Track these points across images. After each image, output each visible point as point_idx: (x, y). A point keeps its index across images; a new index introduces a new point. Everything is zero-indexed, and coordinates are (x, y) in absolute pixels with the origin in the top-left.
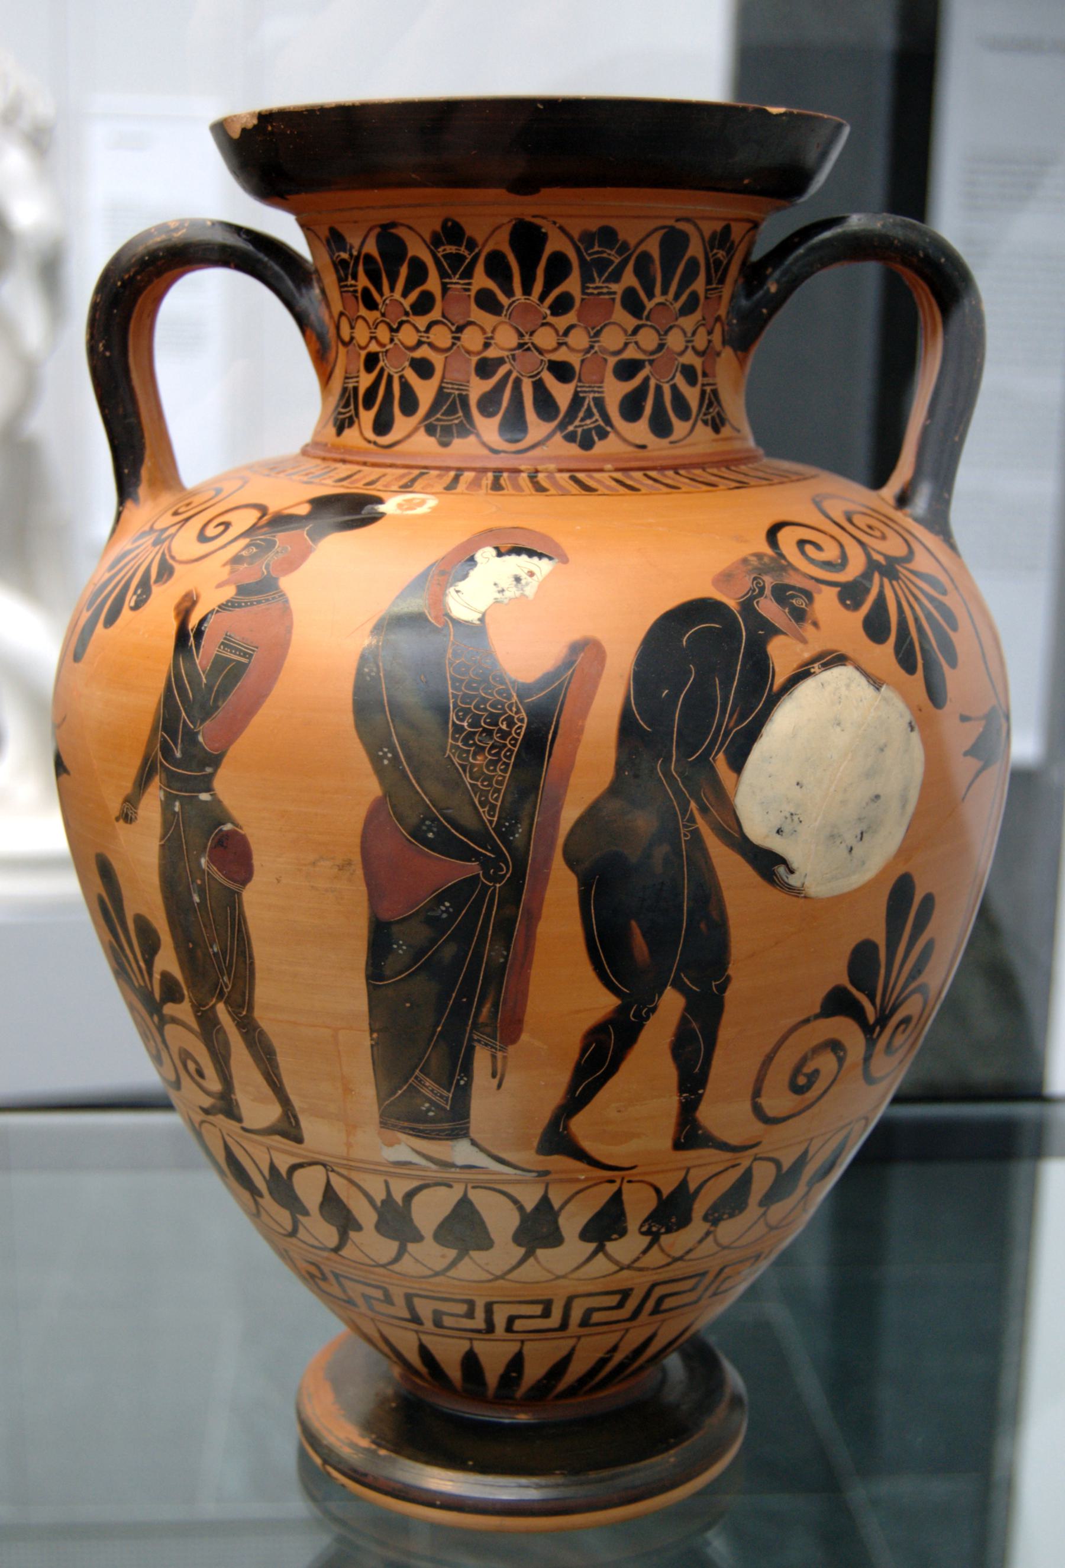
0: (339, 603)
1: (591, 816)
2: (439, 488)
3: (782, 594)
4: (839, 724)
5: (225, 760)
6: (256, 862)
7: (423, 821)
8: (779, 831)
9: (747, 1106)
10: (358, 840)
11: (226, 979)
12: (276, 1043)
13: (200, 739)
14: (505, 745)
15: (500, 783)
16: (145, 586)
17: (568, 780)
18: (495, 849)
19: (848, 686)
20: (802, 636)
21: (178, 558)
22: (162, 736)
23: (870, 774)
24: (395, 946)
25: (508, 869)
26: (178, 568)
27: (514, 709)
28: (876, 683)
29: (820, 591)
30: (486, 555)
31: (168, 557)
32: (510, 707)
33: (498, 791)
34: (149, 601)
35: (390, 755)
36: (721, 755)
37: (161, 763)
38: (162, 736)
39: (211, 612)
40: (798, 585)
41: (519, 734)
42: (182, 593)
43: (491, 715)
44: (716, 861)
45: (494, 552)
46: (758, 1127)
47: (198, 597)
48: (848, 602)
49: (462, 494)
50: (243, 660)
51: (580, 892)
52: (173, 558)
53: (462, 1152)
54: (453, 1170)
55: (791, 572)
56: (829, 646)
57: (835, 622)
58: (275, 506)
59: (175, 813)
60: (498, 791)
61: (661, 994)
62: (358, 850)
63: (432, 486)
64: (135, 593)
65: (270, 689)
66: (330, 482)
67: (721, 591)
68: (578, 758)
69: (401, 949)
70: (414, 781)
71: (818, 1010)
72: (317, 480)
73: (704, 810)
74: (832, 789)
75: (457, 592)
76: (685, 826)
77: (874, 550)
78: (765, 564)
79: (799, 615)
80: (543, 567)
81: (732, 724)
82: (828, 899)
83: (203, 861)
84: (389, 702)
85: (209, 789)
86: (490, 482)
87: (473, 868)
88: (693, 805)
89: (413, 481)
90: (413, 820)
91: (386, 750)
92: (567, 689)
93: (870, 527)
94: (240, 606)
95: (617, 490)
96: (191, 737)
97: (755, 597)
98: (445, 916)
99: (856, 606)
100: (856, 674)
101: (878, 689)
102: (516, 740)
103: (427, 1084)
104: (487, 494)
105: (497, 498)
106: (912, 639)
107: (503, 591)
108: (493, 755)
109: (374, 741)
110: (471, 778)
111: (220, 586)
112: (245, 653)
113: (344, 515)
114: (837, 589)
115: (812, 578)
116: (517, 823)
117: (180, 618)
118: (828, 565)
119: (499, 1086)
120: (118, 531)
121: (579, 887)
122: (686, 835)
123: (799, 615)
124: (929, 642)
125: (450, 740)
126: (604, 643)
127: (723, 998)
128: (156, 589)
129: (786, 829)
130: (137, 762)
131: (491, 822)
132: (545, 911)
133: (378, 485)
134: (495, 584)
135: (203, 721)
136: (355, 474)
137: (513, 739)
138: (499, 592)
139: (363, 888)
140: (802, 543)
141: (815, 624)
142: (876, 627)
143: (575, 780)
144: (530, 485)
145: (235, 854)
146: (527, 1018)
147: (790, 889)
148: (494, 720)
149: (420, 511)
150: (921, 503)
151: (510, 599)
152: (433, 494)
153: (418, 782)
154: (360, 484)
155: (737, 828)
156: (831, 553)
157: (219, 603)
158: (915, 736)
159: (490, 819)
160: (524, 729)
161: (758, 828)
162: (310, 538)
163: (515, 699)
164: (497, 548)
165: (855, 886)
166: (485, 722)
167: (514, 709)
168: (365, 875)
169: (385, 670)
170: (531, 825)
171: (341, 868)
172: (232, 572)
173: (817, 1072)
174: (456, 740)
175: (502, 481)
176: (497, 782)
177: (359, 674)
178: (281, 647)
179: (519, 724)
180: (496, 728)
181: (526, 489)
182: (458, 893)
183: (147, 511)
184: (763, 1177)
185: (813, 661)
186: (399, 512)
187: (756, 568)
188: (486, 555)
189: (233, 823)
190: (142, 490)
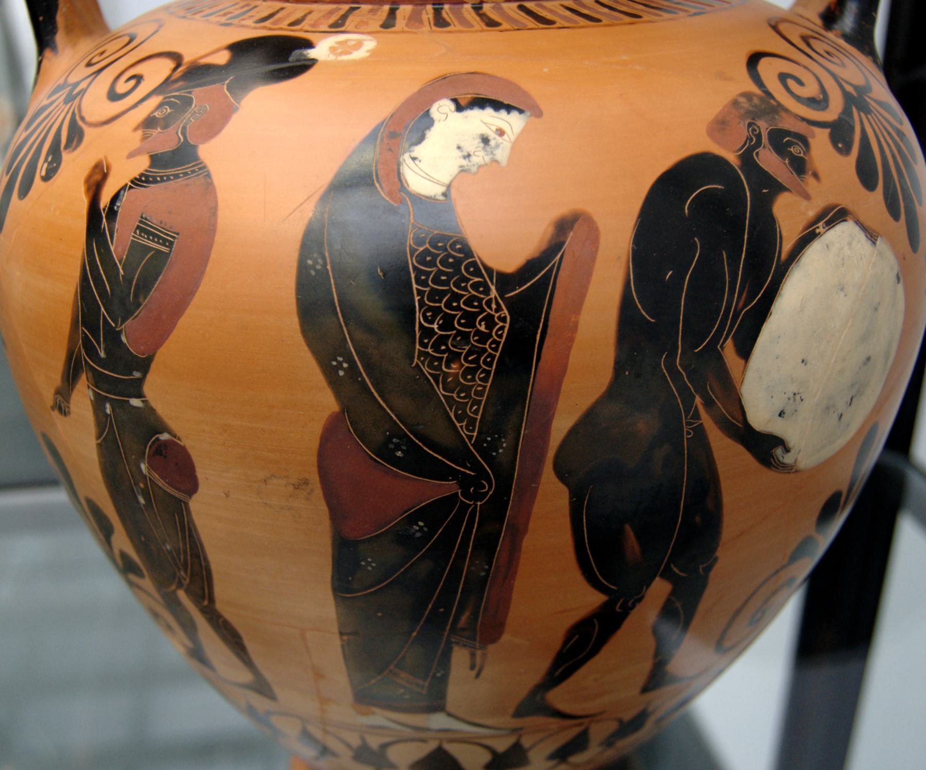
0: (273, 172)
2: (375, 25)
3: (781, 141)
4: (842, 289)
5: (154, 366)
6: (200, 473)
7: (389, 440)
10: (314, 459)
11: (182, 573)
12: (241, 630)
13: (124, 339)
14: (485, 350)
15: (480, 394)
16: (55, 152)
18: (477, 467)
21: (89, 118)
22: (83, 332)
23: (865, 337)
24: (363, 563)
25: (490, 487)
26: (87, 131)
27: (494, 306)
30: (442, 109)
31: (77, 118)
32: (489, 303)
33: (478, 403)
34: (60, 170)
35: (345, 365)
36: (729, 341)
37: (86, 362)
38: (83, 332)
39: (124, 188)
41: (500, 336)
42: (93, 163)
43: (466, 315)
44: (717, 454)
45: (452, 106)
47: (108, 168)
49: (403, 32)
50: (163, 249)
52: (82, 118)
53: (438, 721)
55: (783, 114)
58: (189, 55)
59: (107, 415)
63: (367, 24)
64: (46, 160)
65: (197, 286)
66: (249, 22)
67: (718, 143)
68: (571, 360)
69: (370, 565)
70: (376, 395)
72: (236, 21)
73: (709, 403)
75: (414, 159)
76: (688, 424)
78: (755, 106)
79: (799, 166)
80: (513, 123)
81: (741, 304)
83: (143, 467)
84: (339, 301)
85: (140, 395)
86: (431, 16)
87: (450, 487)
88: (698, 400)
89: (344, 17)
91: (340, 359)
92: (556, 278)
93: (828, 53)
94: (155, 182)
95: (576, 22)
96: (113, 337)
98: (418, 535)
100: (856, 229)
101: (874, 243)
102: (498, 343)
104: (432, 32)
105: (442, 37)
107: (469, 156)
108: (471, 362)
109: (326, 350)
110: (444, 389)
111: (131, 155)
112: (165, 240)
113: (269, 63)
114: (828, 130)
115: (803, 119)
116: (500, 437)
117: (91, 193)
118: (811, 102)
119: (478, 675)
120: (39, 80)
121: (571, 498)
122: (688, 433)
124: (906, 183)
125: (418, 347)
126: (596, 218)
128: (66, 156)
129: (787, 411)
130: (62, 355)
131: (470, 438)
132: (531, 525)
133: (305, 25)
134: (459, 148)
135: (124, 319)
136: (278, 12)
137: (494, 342)
138: (464, 157)
139: (324, 508)
143: (568, 385)
144: (478, 18)
145: (178, 466)
146: (509, 621)
148: (470, 319)
149: (359, 54)
150: (848, 21)
151: (480, 167)
152: (369, 33)
154: (284, 25)
155: (741, 418)
156: (810, 90)
157: (132, 177)
158: (900, 287)
161: (760, 414)
162: (230, 92)
163: (494, 293)
164: (455, 101)
166: (459, 323)
167: (494, 306)
169: (332, 262)
171: (296, 487)
172: (145, 138)
174: (425, 346)
175: (444, 15)
176: (476, 393)
177: (302, 270)
178: (207, 230)
179: (501, 324)
180: (473, 330)
181: (474, 23)
182: (433, 513)
183: (67, 60)
186: (332, 57)
187: (748, 112)
188: (442, 109)
189: (170, 432)
190: (60, 38)
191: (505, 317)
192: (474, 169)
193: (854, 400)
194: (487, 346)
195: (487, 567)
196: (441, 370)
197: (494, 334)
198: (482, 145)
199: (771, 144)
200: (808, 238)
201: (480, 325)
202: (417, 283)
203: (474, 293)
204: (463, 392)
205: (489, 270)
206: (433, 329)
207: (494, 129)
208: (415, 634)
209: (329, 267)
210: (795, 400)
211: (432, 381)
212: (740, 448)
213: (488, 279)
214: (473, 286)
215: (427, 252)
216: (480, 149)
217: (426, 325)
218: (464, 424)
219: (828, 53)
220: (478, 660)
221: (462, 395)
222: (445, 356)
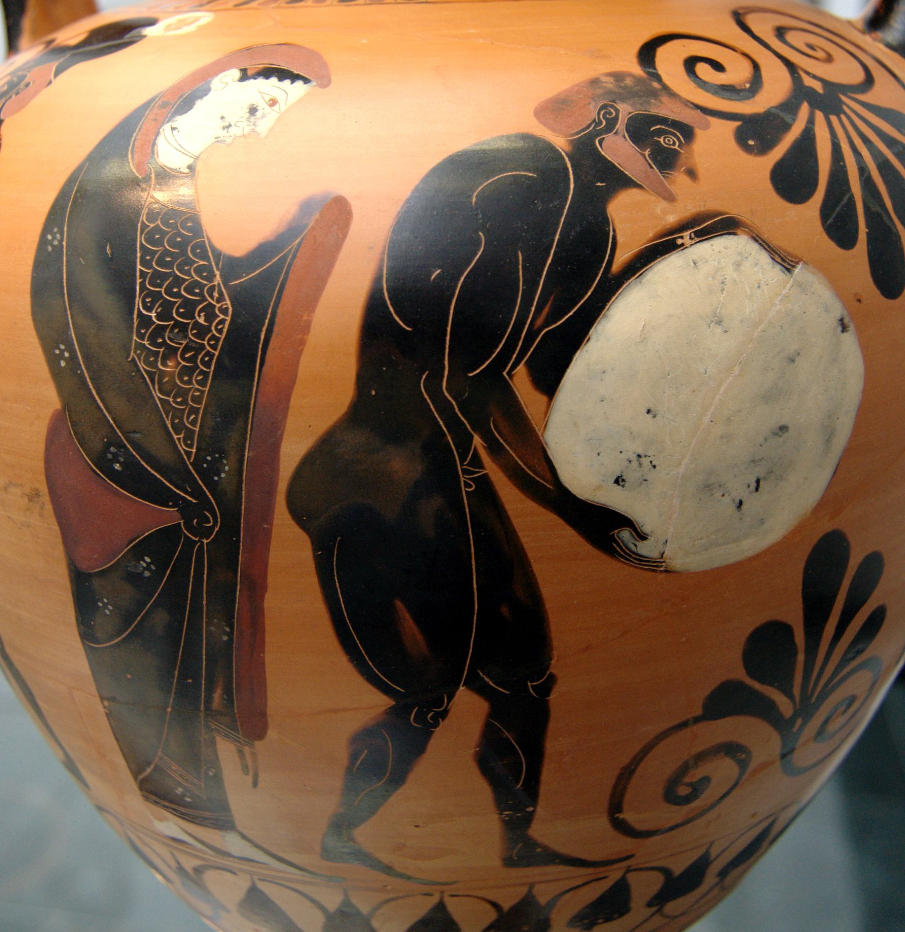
1: (324, 450)
3: (642, 130)
4: (719, 322)
8: (618, 481)
9: (603, 822)
17: (288, 399)
18: (196, 492)
19: (738, 265)
20: (667, 190)
23: (770, 396)
24: (100, 604)
27: (216, 295)
28: (786, 261)
29: (707, 126)
32: (211, 290)
36: (521, 369)
40: (672, 117)
43: (187, 303)
46: (625, 844)
48: (751, 142)
51: (316, 558)
54: (231, 859)
55: (665, 99)
56: (711, 205)
57: (723, 167)
60: (195, 411)
61: (451, 697)
62: (43, 478)
67: (545, 124)
68: (301, 368)
71: (699, 712)
73: (494, 448)
74: (706, 419)
76: (465, 472)
77: (808, 73)
78: (625, 87)
81: (539, 322)
82: (705, 573)
87: (170, 515)
88: (477, 441)
90: (97, 445)
92: (290, 266)
93: (812, 47)
97: (599, 133)
99: (764, 147)
100: (754, 247)
102: (218, 339)
103: (174, 768)
106: (852, 196)
110: (161, 391)
116: (221, 458)
118: (728, 90)
119: (255, 784)
121: (315, 550)
123: (665, 160)
125: (135, 338)
127: (547, 702)
129: (630, 477)
132: (271, 580)
137: (213, 337)
139: (56, 527)
140: (691, 63)
141: (692, 173)
142: (792, 180)
147: (642, 561)
148: (189, 308)
153: (98, 394)
155: (548, 475)
156: (737, 73)
158: (849, 340)
159: (187, 450)
160: (227, 324)
163: (218, 279)
165: (749, 554)
166: (178, 314)
167: (216, 295)
168: (55, 510)
170: (241, 461)
173: (706, 780)
176: (194, 399)
179: (222, 317)
184: (643, 886)
185: (682, 227)
187: (609, 92)
191: (227, 309)
192: (229, 140)
193: (761, 483)
194: (205, 343)
195: (212, 628)
196: (157, 367)
197: (213, 328)
198: (248, 115)
199: (627, 130)
200: (662, 246)
201: (199, 316)
202: (141, 264)
203: (197, 278)
204: (180, 397)
205: (218, 255)
206: (151, 317)
207: (267, 98)
208: (169, 710)
209: (64, 243)
210: (640, 465)
211: (148, 379)
212: (553, 519)
213: (213, 264)
214: (196, 271)
215: (157, 229)
216: (244, 120)
217: (144, 312)
218: (182, 436)
219: (812, 47)
220: (249, 761)
221: (179, 400)
222: (161, 350)
